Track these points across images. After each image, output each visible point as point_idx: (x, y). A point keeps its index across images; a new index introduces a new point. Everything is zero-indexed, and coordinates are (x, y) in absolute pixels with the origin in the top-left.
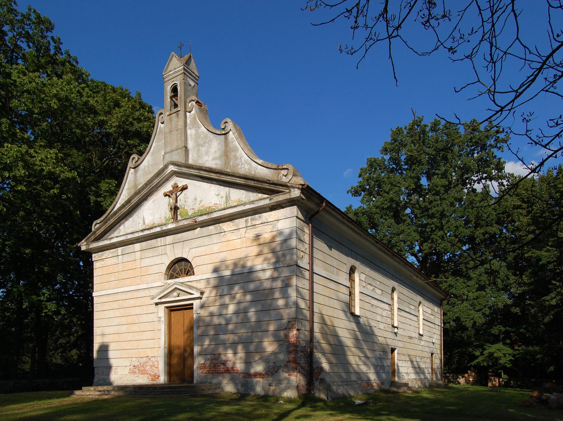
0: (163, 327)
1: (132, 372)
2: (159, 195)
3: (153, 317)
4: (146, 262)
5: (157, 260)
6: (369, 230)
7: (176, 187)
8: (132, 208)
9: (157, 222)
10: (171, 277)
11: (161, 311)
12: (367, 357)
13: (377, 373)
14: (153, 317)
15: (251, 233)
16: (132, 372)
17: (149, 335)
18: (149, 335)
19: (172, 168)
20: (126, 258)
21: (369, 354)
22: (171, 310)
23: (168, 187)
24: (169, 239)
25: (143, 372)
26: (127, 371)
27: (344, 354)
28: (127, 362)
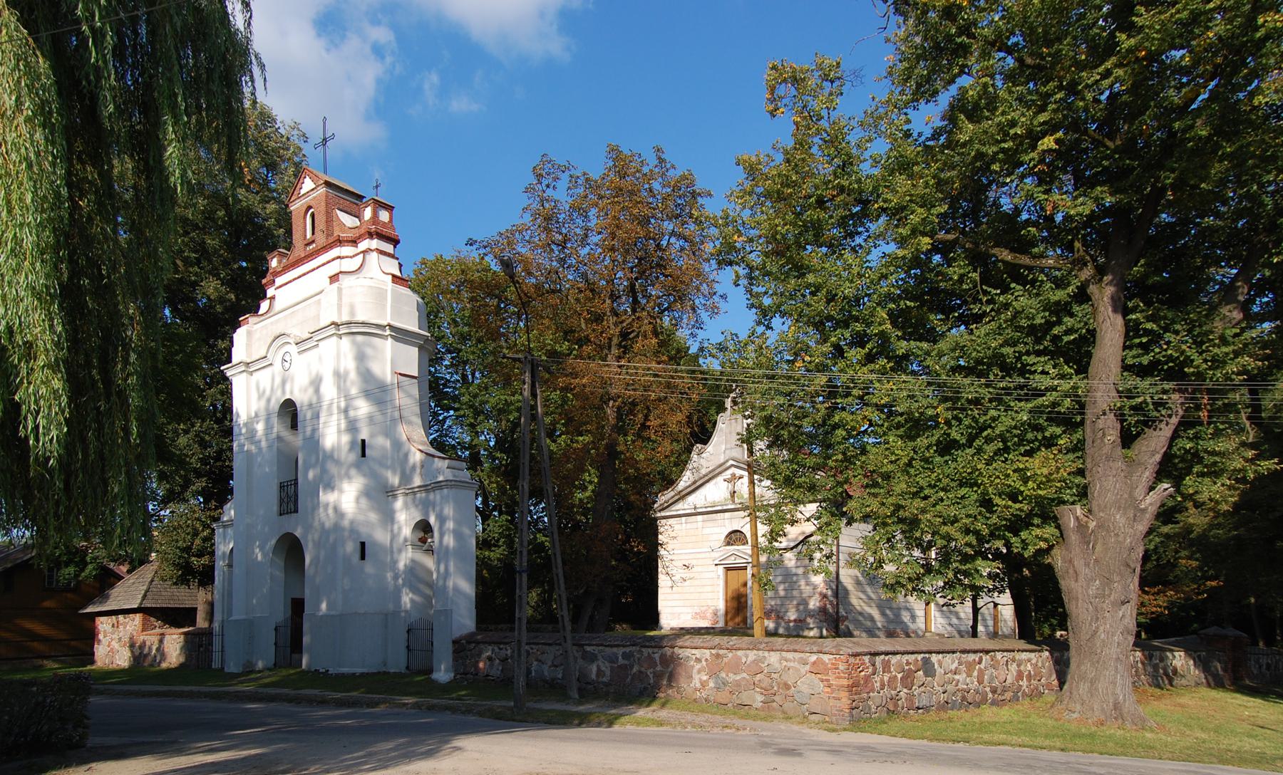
0: (721, 583)
1: (694, 618)
2: (720, 479)
3: (713, 575)
4: (707, 531)
5: (717, 530)
6: (1258, 35)
7: (733, 475)
8: (695, 488)
9: (717, 499)
10: (728, 544)
11: (721, 569)
12: (870, 598)
13: (883, 614)
14: (713, 575)
15: (790, 536)
16: (694, 618)
17: (708, 589)
18: (708, 589)
19: (731, 462)
20: (689, 526)
21: (873, 596)
22: (728, 569)
23: (728, 474)
24: (727, 515)
25: (704, 618)
26: (689, 617)
27: (74, 340)
28: (689, 610)
